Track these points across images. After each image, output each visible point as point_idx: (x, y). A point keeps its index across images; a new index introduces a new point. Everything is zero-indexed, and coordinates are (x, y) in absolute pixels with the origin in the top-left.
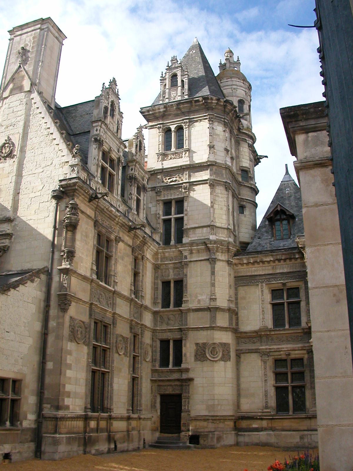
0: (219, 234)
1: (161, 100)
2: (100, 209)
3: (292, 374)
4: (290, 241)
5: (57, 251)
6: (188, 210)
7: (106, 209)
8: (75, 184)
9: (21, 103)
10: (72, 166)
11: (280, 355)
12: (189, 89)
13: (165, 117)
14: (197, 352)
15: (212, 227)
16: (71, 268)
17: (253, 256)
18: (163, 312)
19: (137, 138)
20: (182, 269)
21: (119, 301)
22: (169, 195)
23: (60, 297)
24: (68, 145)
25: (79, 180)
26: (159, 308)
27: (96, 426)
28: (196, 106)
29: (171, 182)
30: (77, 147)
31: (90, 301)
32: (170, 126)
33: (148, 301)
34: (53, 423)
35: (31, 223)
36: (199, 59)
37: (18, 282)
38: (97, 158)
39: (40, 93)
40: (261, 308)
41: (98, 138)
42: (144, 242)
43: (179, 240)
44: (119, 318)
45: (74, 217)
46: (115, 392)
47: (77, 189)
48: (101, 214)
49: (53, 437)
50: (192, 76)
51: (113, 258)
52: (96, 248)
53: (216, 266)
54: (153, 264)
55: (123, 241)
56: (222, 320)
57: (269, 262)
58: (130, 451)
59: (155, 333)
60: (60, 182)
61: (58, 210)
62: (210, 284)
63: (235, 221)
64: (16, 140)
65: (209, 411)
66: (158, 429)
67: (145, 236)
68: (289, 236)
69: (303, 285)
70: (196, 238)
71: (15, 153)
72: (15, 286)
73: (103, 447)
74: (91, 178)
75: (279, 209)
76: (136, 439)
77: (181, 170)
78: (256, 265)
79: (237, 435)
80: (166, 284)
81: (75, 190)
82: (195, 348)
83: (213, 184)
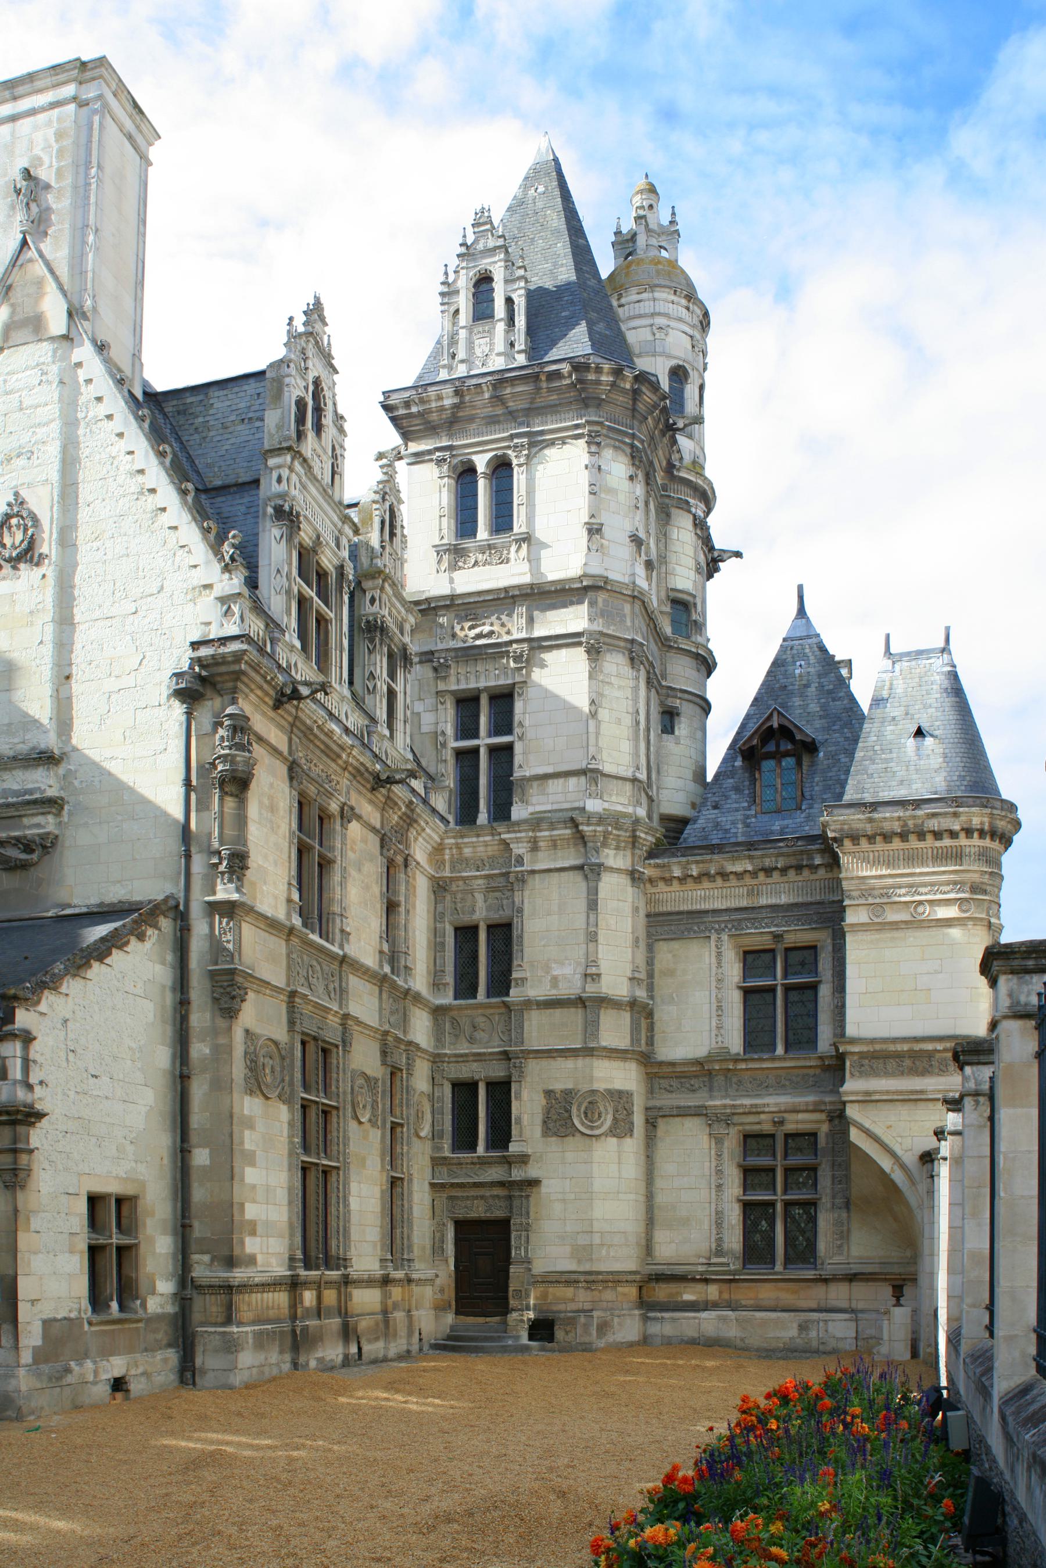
0: (611, 795)
1: (444, 367)
2: (303, 728)
3: (787, 1171)
4: (800, 817)
5: (199, 852)
6: (527, 723)
7: (318, 727)
8: (238, 657)
9: (44, 378)
10: (223, 600)
11: (759, 1123)
12: (530, 331)
13: (456, 427)
15: (591, 774)
16: (244, 899)
17: (698, 858)
18: (460, 1008)
19: (384, 499)
20: (509, 894)
21: (354, 982)
22: (473, 678)
23: (218, 978)
24: (206, 531)
25: (249, 644)
26: (447, 999)
27: (314, 1303)
29: (480, 636)
30: (234, 537)
31: (288, 985)
33: (419, 982)
34: (222, 1298)
35: (113, 767)
36: (556, 220)
37: (108, 941)
38: (286, 569)
39: (101, 348)
41: (287, 508)
42: (408, 817)
43: (501, 812)
44: (356, 1028)
45: (241, 756)
46: (354, 1219)
47: (243, 673)
48: (304, 740)
49: (225, 1332)
50: (536, 282)
51: (337, 867)
52: (296, 841)
53: (601, 885)
54: (432, 878)
55: (359, 818)
56: (615, 1030)
57: (739, 876)
58: (391, 1360)
59: (439, 1064)
60: (194, 649)
61: (193, 733)
62: (585, 933)
63: (652, 757)
64: (42, 503)
65: (579, 1262)
66: (450, 1306)
67: (414, 800)
68: (800, 800)
69: (829, 941)
70: (549, 807)
71: (45, 550)
72: (102, 951)
73: (333, 1351)
74: (276, 635)
75: (776, 725)
76: (402, 1331)
77: (505, 600)
78: (706, 884)
79: (645, 1319)
80: (466, 934)
81: (238, 675)
82: (544, 1102)
83: (595, 647)
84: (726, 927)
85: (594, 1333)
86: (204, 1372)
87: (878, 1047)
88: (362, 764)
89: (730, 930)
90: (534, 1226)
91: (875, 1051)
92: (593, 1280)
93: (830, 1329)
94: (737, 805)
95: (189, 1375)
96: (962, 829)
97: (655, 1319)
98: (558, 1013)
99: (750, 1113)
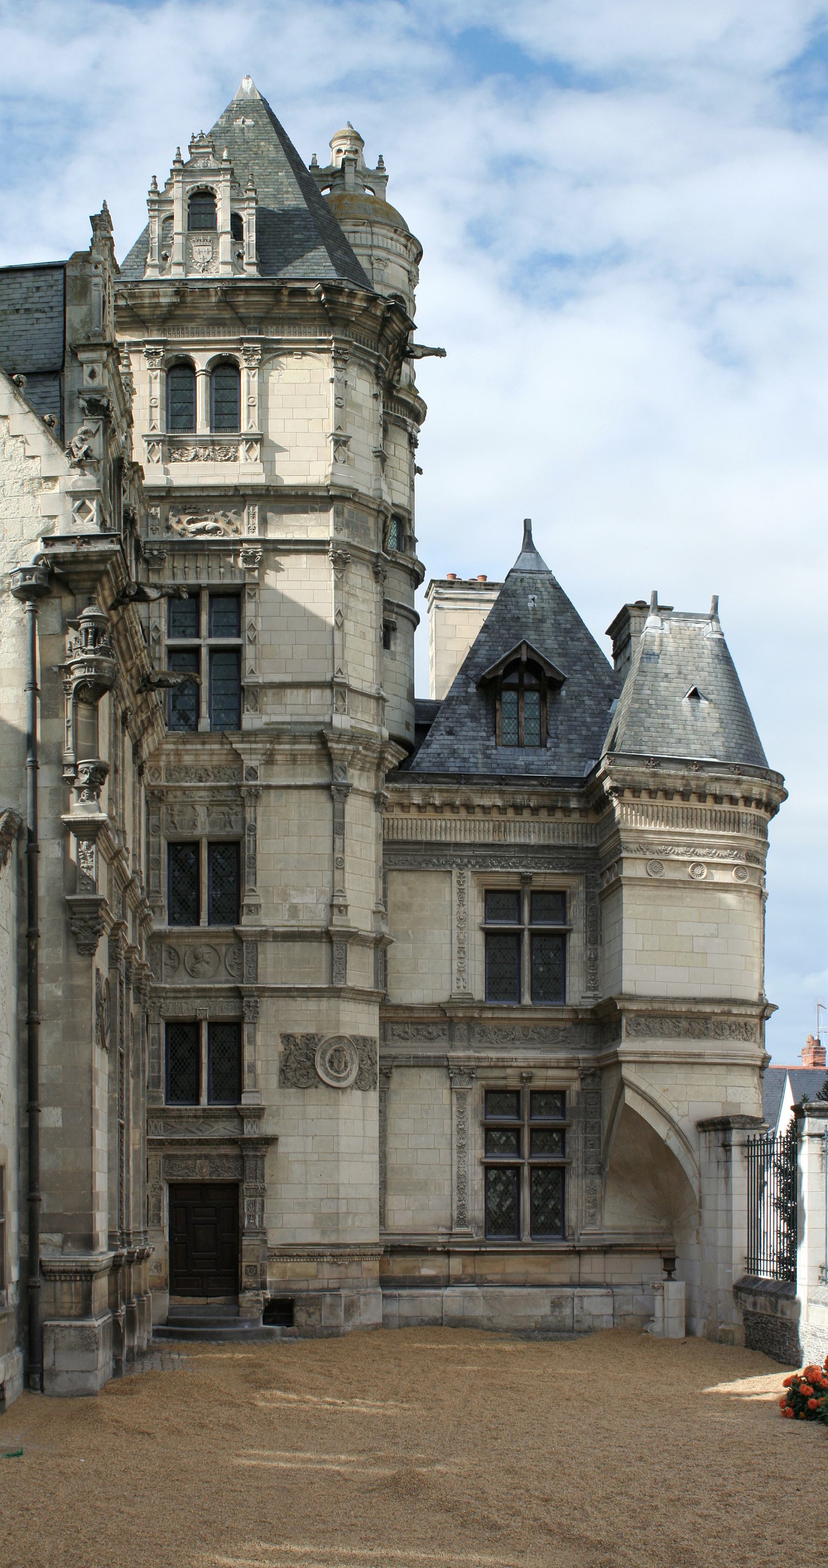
0: (356, 712)
3: (533, 1131)
4: (545, 756)
5: (47, 763)
6: (259, 627)
10: (75, 495)
11: (504, 1078)
13: (170, 324)
14: (286, 1061)
15: (336, 687)
17: (443, 787)
18: (180, 935)
20: (239, 809)
22: (204, 575)
28: (290, 304)
32: (192, 354)
34: (78, 1286)
40: (455, 940)
43: (229, 719)
49: (82, 1327)
53: (347, 807)
56: (359, 972)
57: (485, 809)
62: (314, 859)
65: (323, 1233)
69: (581, 888)
70: (287, 719)
75: (524, 658)
77: (235, 498)
78: (448, 815)
80: (182, 852)
82: (281, 1048)
84: (469, 862)
85: (342, 1314)
86: (54, 1374)
87: (656, 1006)
89: (473, 866)
90: (269, 1192)
91: (653, 1010)
92: (340, 1254)
93: (585, 1306)
94: (475, 734)
95: (37, 1377)
96: (743, 797)
98: (297, 947)
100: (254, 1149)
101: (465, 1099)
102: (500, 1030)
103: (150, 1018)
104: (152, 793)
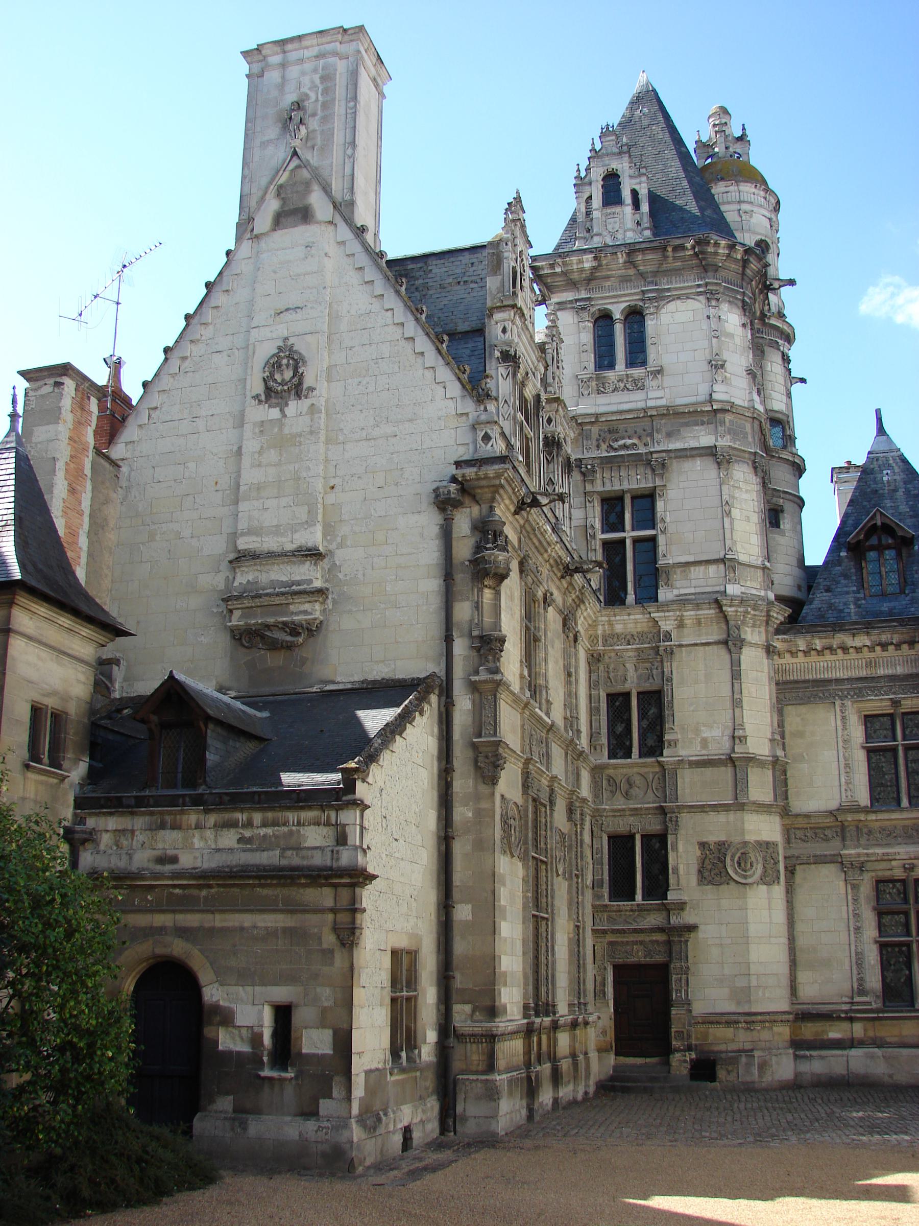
5: (461, 637)
6: (668, 519)
15: (727, 562)
18: (615, 767)
47: (502, 486)
49: (487, 1080)
53: (742, 657)
56: (760, 787)
57: (858, 650)
62: (727, 700)
65: (738, 1003)
66: (612, 1047)
70: (692, 591)
75: (879, 523)
78: (828, 657)
80: (618, 703)
82: (698, 853)
84: (848, 694)
86: (464, 1119)
88: (559, 557)
89: (852, 697)
92: (750, 1019)
97: (805, 1057)
98: (708, 772)
99: (882, 860)
100: (677, 936)
101: (858, 889)
102: (884, 830)
103: (595, 834)
104: (592, 656)
